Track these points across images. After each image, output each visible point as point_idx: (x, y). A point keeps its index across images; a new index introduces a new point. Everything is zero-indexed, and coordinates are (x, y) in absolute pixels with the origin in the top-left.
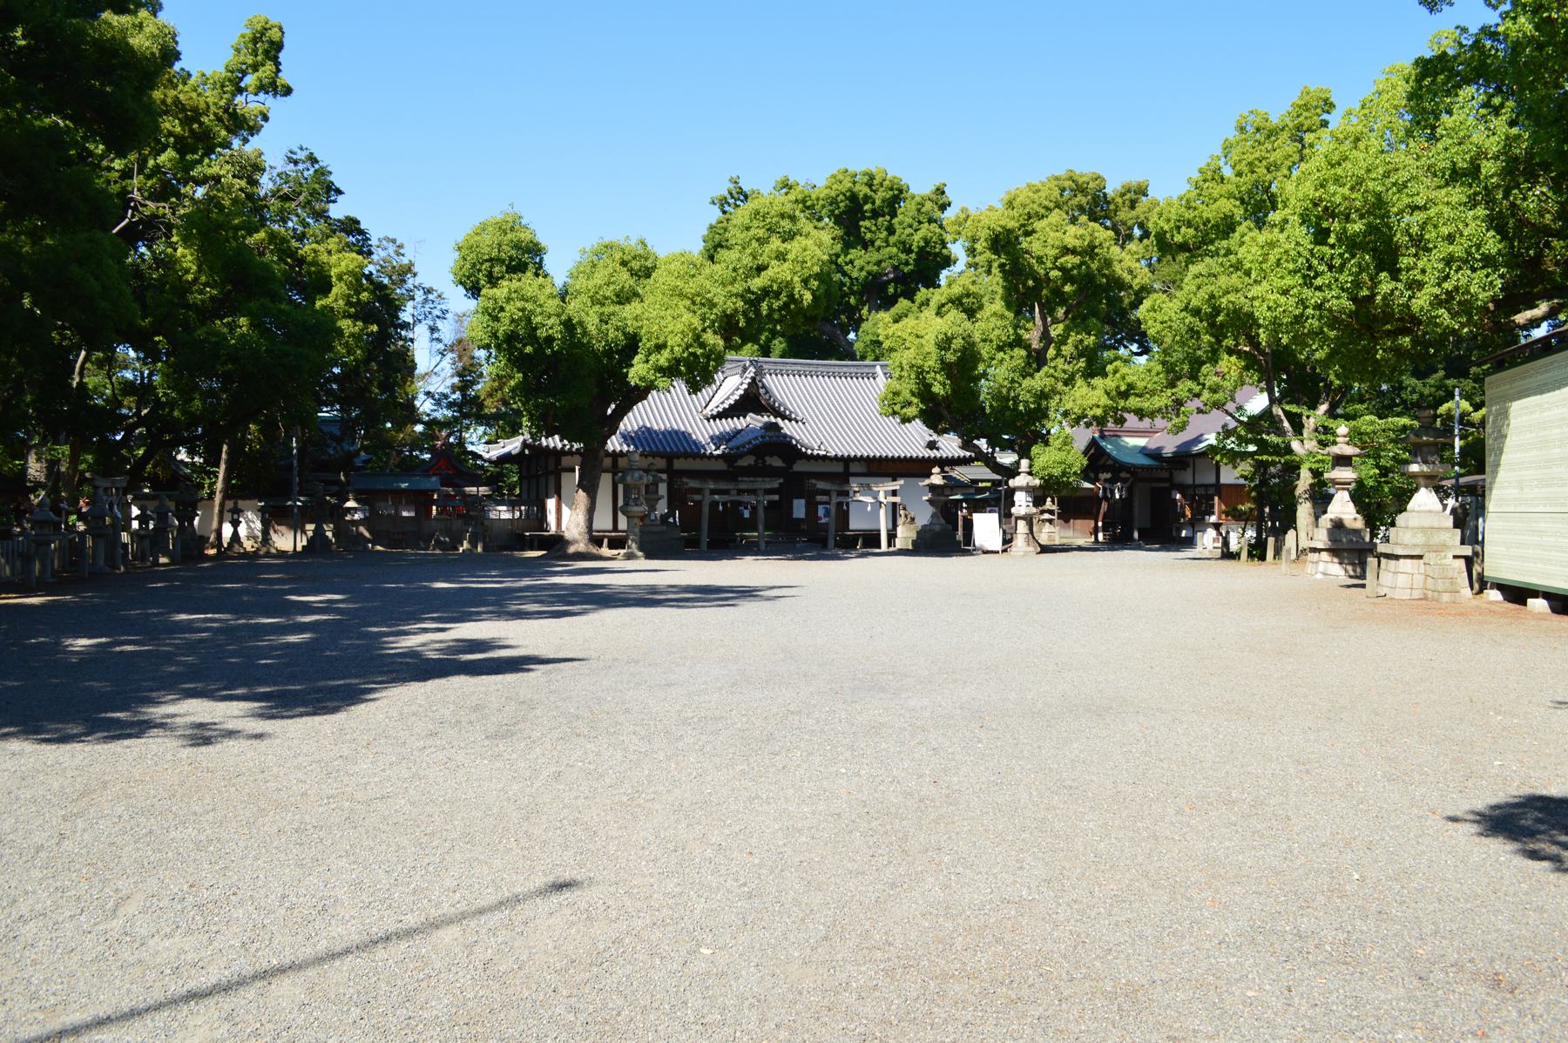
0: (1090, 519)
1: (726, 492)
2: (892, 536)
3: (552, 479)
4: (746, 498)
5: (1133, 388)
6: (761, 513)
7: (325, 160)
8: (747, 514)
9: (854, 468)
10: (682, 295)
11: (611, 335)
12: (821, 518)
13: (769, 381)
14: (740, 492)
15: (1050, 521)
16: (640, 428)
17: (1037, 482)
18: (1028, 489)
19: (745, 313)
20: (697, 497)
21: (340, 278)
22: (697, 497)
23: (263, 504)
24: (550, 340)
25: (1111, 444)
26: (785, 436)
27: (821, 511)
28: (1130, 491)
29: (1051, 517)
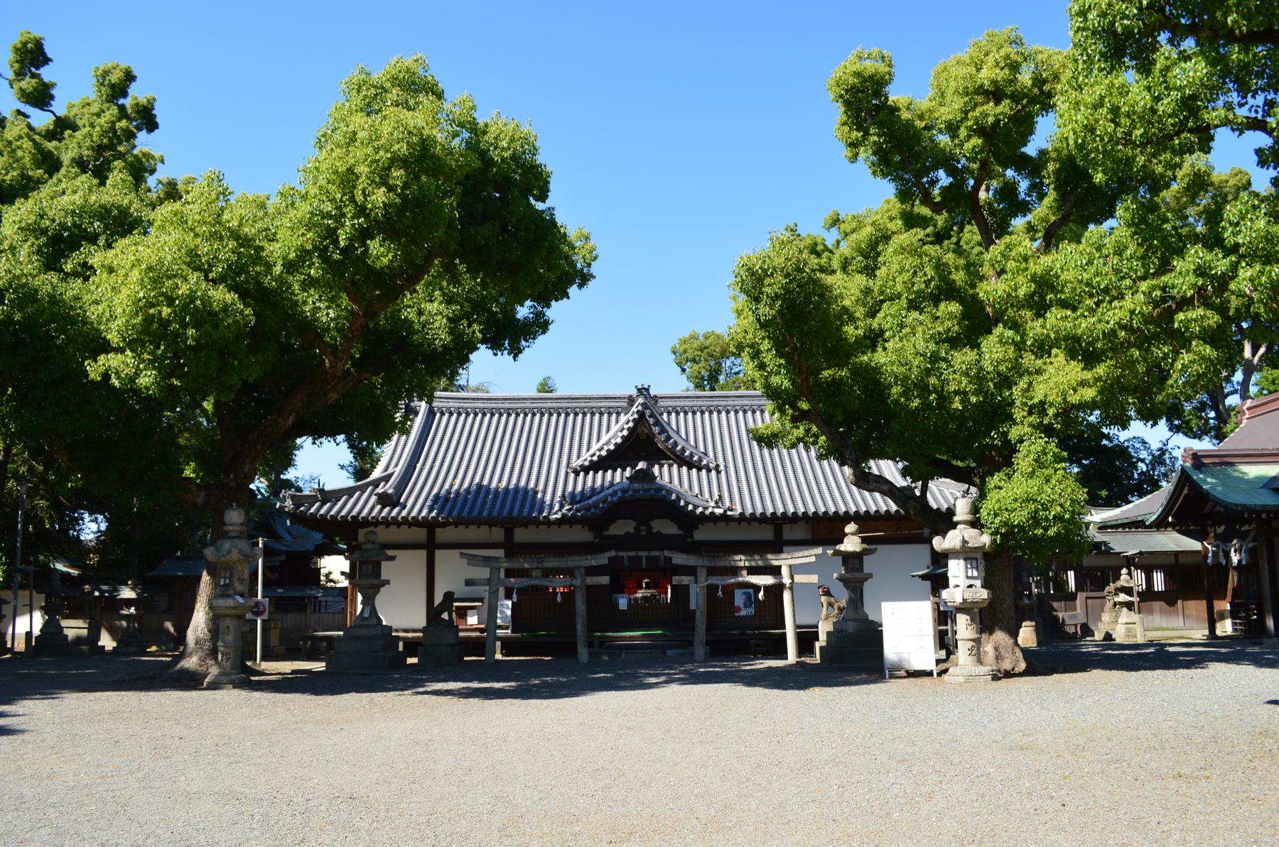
0: (1201, 599)
5: (1053, 288)
12: (739, 609)
15: (1129, 606)
16: (526, 490)
17: (986, 539)
25: (1213, 476)
28: (1252, 553)
29: (1129, 598)
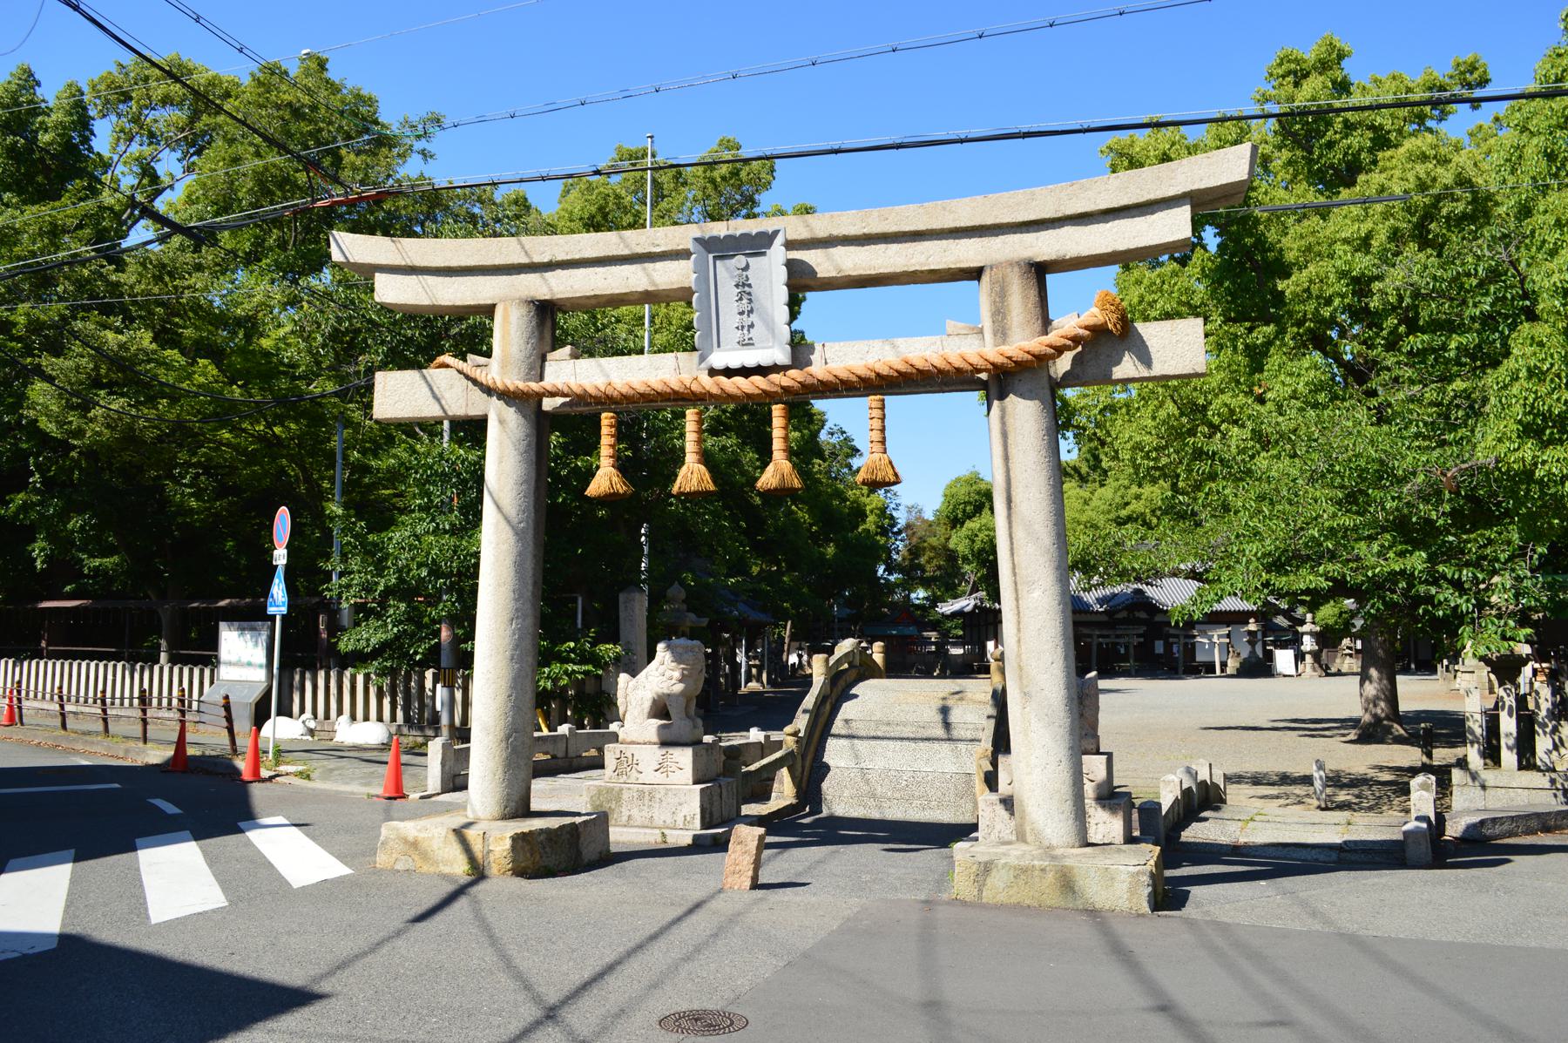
1: (1108, 636)
2: (1224, 665)
3: (991, 628)
6: (1132, 651)
7: (850, 432)
8: (1122, 651)
14: (1118, 636)
17: (1318, 629)
18: (1311, 633)
20: (1089, 640)
21: (872, 511)
22: (1089, 640)
26: (1148, 597)
27: (1175, 649)
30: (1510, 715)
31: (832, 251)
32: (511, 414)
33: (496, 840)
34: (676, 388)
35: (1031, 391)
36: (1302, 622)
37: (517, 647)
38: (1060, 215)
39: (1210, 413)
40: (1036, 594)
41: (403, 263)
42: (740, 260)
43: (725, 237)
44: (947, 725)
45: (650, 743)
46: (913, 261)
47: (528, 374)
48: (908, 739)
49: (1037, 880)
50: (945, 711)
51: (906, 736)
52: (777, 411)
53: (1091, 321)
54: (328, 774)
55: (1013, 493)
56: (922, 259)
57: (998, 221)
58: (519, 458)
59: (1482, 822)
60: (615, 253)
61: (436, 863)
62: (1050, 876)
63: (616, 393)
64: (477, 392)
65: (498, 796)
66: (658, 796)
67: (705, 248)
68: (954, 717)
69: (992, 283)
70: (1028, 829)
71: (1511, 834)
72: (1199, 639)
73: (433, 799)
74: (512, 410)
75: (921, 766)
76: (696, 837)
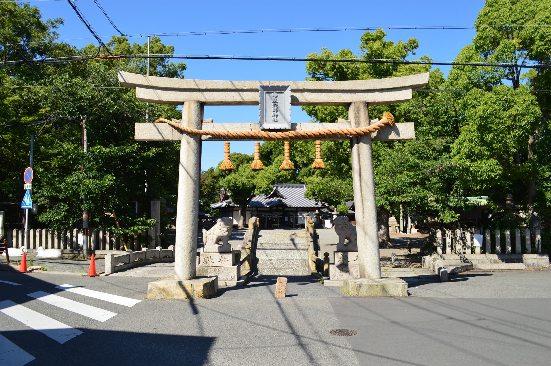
3: (231, 213)
4: (274, 217)
9: (299, 210)
10: (264, 177)
11: (250, 184)
13: (279, 189)
18: (336, 214)
19: (277, 180)
23: (459, 215)
24: (240, 187)
27: (291, 219)
30: (450, 238)
31: (304, 93)
32: (192, 140)
33: (197, 286)
34: (253, 135)
35: (367, 142)
36: (333, 211)
37: (194, 220)
38: (375, 89)
39: (344, 145)
40: (368, 203)
41: (148, 85)
42: (274, 94)
43: (271, 86)
44: (295, 245)
45: (216, 252)
46: (330, 99)
47: (197, 127)
48: (283, 249)
49: (375, 288)
50: (292, 240)
51: (282, 248)
52: (286, 143)
53: (385, 122)
54: (52, 268)
55: (362, 172)
56: (333, 98)
57: (356, 89)
58: (194, 155)
59: (455, 268)
60: (230, 88)
61: (173, 295)
62: (379, 288)
63: (231, 135)
64: (176, 132)
65: (188, 272)
66: (221, 270)
67: (263, 89)
68: (297, 241)
69: (355, 108)
70: (366, 274)
71: (461, 272)
72: (300, 216)
73: (109, 276)
74: (192, 139)
75: (289, 258)
76: (237, 283)
